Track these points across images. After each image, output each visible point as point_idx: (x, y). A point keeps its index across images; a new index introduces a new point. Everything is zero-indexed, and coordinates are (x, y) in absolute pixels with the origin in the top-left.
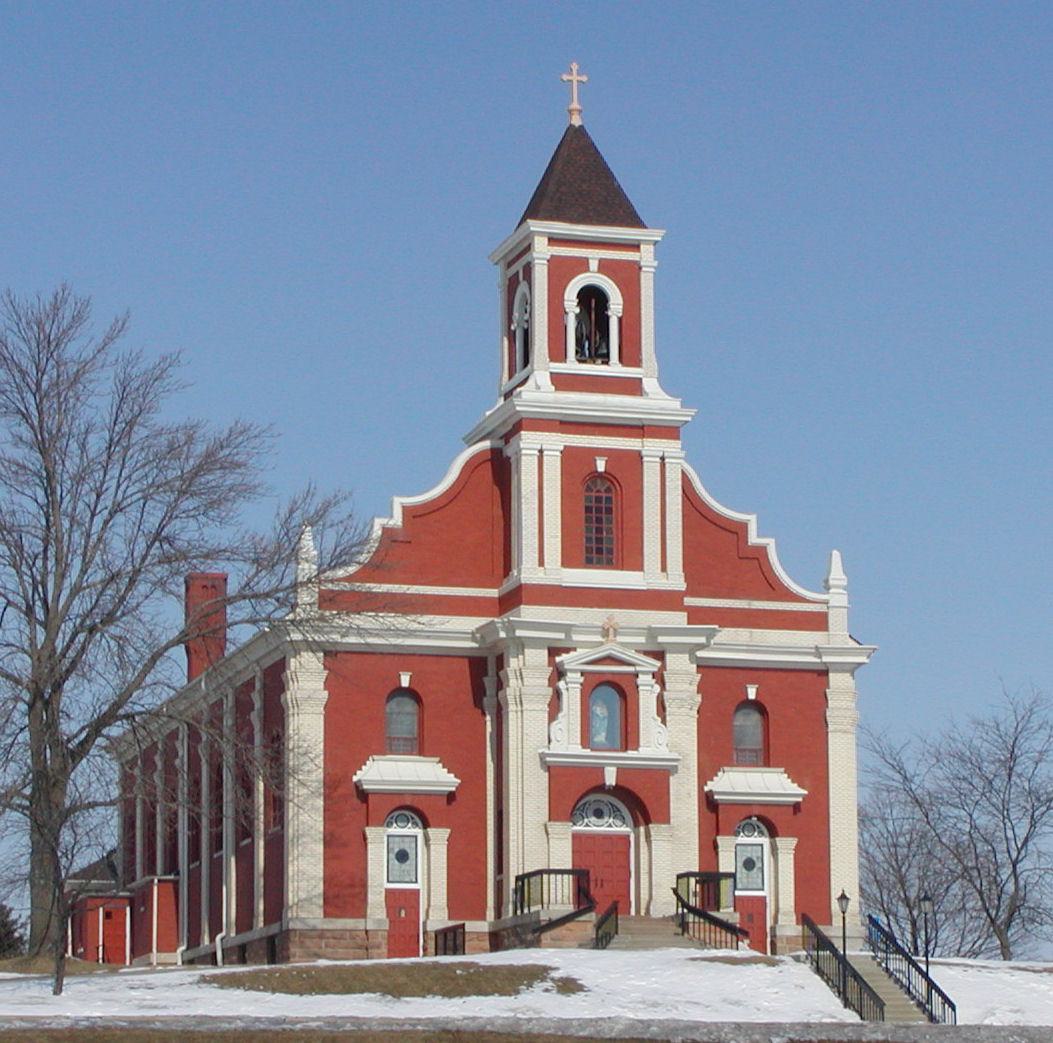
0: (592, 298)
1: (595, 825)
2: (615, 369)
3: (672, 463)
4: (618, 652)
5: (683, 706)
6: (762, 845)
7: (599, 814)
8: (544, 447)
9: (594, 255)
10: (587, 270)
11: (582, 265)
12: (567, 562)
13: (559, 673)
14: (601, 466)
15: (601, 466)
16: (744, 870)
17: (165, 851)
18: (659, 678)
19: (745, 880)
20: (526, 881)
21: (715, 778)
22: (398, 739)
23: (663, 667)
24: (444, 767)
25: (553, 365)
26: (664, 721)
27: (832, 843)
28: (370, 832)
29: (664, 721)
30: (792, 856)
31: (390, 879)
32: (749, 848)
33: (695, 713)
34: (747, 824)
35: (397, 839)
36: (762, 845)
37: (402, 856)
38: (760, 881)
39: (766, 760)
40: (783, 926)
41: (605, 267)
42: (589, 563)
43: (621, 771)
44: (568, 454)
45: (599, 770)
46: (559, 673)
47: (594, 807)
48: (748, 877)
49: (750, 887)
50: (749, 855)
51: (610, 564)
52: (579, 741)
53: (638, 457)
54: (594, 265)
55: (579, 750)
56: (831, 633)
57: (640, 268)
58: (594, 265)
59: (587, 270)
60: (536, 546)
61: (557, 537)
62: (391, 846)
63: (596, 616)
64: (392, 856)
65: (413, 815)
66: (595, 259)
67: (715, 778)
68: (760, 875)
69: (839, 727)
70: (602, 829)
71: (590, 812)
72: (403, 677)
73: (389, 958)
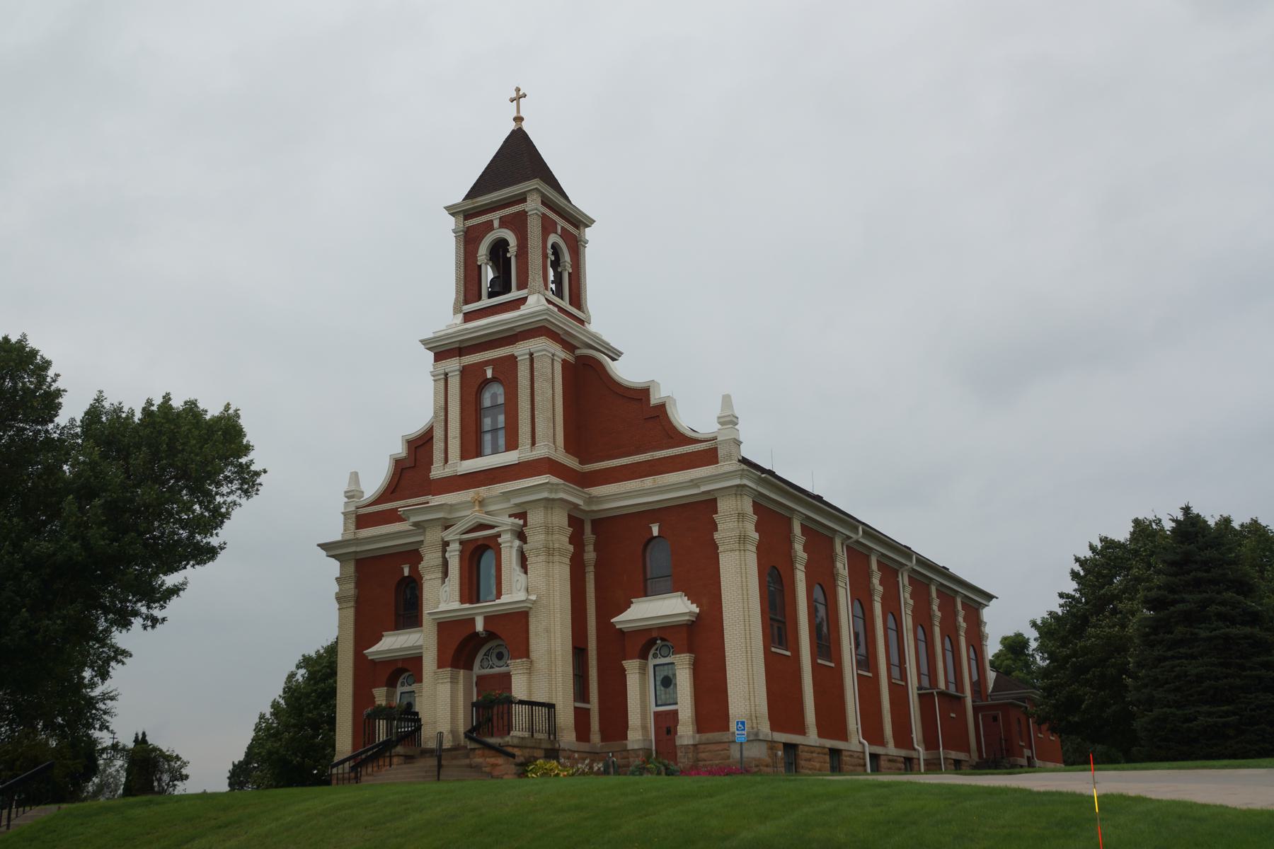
0: (499, 248)
6: (655, 666)
9: (495, 217)
11: (489, 226)
16: (662, 688)
18: (521, 536)
19: (663, 697)
20: (893, 681)
23: (525, 524)
24: (688, 599)
28: (626, 664)
29: (526, 573)
31: (659, 703)
32: (666, 667)
33: (568, 561)
40: (681, 737)
41: (504, 223)
43: (488, 619)
44: (465, 372)
45: (472, 621)
48: (666, 694)
49: (668, 702)
50: (666, 674)
54: (496, 224)
55: (456, 605)
56: (354, 515)
58: (496, 224)
61: (456, 437)
67: (690, 602)
69: (727, 547)
71: (494, 657)
73: (924, 760)
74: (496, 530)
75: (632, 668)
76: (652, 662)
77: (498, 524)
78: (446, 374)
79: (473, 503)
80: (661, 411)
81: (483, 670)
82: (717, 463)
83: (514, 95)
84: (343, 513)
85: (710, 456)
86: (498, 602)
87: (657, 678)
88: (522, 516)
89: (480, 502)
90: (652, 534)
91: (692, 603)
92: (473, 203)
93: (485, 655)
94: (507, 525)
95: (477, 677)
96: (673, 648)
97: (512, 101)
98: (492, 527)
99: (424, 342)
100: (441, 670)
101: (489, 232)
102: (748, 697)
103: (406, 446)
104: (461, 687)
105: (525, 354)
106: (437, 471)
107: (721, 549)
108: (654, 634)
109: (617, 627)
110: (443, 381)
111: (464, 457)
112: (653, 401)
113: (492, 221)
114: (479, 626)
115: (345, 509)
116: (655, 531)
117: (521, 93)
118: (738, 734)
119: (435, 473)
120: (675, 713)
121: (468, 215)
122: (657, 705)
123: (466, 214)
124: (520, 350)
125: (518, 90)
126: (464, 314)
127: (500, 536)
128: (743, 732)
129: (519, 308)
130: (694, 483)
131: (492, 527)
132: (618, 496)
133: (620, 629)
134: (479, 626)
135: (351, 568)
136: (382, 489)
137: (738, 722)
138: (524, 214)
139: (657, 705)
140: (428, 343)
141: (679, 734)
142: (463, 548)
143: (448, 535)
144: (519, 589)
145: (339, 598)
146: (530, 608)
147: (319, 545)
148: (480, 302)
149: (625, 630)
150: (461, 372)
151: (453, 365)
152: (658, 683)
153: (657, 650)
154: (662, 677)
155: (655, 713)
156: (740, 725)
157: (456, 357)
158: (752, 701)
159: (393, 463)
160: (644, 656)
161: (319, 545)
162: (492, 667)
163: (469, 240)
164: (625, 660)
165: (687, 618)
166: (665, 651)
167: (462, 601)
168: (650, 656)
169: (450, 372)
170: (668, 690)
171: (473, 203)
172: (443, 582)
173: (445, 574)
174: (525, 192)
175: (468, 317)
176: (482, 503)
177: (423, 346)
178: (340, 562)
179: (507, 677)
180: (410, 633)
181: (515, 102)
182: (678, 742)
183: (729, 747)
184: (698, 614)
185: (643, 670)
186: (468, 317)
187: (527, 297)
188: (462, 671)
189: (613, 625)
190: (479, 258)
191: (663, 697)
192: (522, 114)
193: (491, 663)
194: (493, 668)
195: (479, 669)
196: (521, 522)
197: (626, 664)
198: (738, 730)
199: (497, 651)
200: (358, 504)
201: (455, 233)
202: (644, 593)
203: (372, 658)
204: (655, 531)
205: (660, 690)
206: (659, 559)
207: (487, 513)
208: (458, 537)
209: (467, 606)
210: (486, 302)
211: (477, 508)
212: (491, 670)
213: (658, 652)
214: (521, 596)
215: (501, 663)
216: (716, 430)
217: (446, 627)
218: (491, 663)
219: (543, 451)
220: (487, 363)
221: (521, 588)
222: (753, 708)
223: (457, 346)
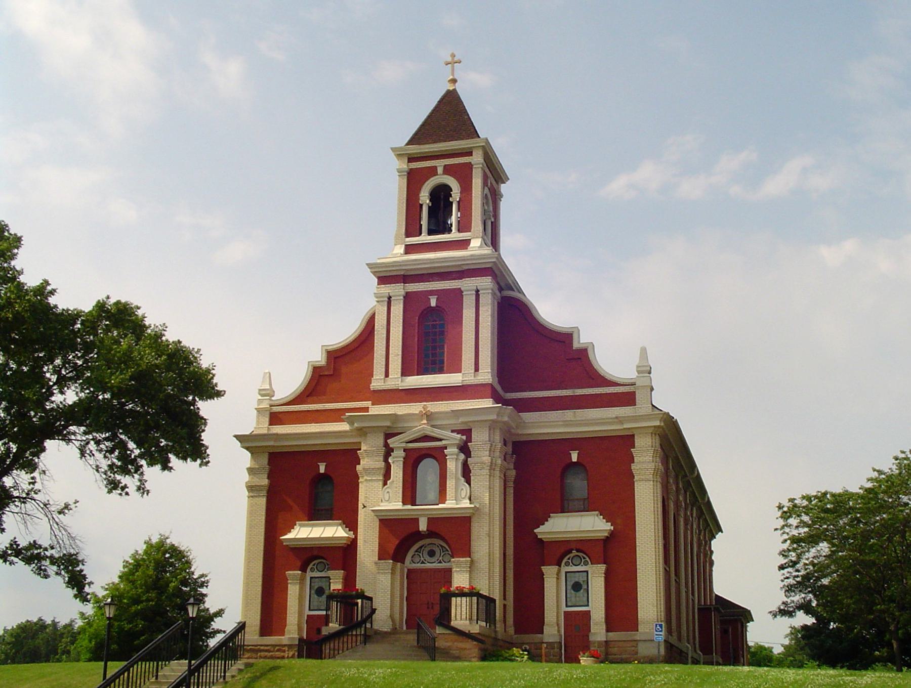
0: (441, 196)
1: (428, 562)
2: (454, 235)
3: (484, 293)
4: (436, 433)
5: (483, 468)
6: (311, 578)
7: (432, 554)
8: (391, 295)
9: (440, 164)
10: (436, 174)
11: (433, 171)
12: (405, 372)
13: (388, 451)
14: (433, 303)
15: (433, 303)
17: (701, 582)
18: (465, 449)
19: (573, 599)
21: (605, 520)
22: (322, 510)
25: (408, 239)
26: (385, 484)
27: (638, 567)
28: (545, 569)
30: (603, 579)
31: (569, 604)
34: (321, 562)
35: (317, 579)
36: (311, 578)
37: (577, 587)
38: (585, 599)
39: (588, 506)
40: (595, 634)
41: (448, 170)
42: (423, 370)
43: (431, 521)
44: (408, 298)
45: (416, 521)
46: (388, 451)
47: (428, 549)
50: (577, 580)
51: (441, 371)
52: (401, 500)
53: (459, 293)
54: (440, 170)
57: (472, 166)
58: (440, 170)
59: (436, 174)
60: (384, 363)
61: (398, 355)
62: (312, 584)
63: (415, 408)
64: (313, 592)
65: (585, 556)
66: (441, 166)
67: (605, 520)
68: (586, 595)
70: (434, 564)
72: (321, 467)
74: (444, 442)
75: (549, 572)
76: (565, 569)
77: (445, 438)
78: (390, 298)
79: (421, 416)
80: (583, 355)
81: (414, 564)
82: (635, 405)
83: (449, 59)
84: (256, 409)
85: (628, 399)
86: (441, 506)
87: (568, 583)
88: (467, 432)
89: (427, 416)
90: (571, 460)
91: (607, 522)
92: (420, 149)
93: (416, 551)
94: (456, 439)
95: (408, 570)
96: (328, 565)
97: (447, 64)
98: (441, 440)
99: (370, 266)
100: (383, 561)
101: (432, 177)
102: (655, 604)
103: (325, 355)
104: (398, 577)
105: (473, 290)
106: (378, 382)
107: (636, 478)
108: (573, 546)
109: (539, 537)
110: (474, 296)
111: (405, 372)
112: (576, 345)
113: (436, 167)
114: (423, 526)
115: (258, 405)
116: (574, 457)
117: (456, 59)
118: (657, 635)
119: (375, 384)
120: (587, 614)
121: (411, 159)
122: (567, 606)
123: (410, 157)
124: (467, 285)
125: (453, 56)
126: (406, 245)
127: (446, 448)
128: (661, 633)
129: (467, 249)
130: (619, 420)
131: (441, 440)
132: (552, 424)
133: (541, 540)
134: (423, 526)
135: (264, 460)
136: (299, 392)
137: (656, 625)
138: (469, 166)
139: (567, 606)
140: (374, 268)
141: (592, 631)
142: (406, 455)
143: (394, 442)
144: (463, 497)
145: (251, 488)
146: (474, 514)
147: (236, 436)
148: (420, 237)
149: (545, 540)
150: (404, 297)
151: (398, 290)
152: (569, 587)
153: (569, 559)
154: (572, 583)
155: (565, 612)
156: (658, 627)
157: (401, 283)
158: (659, 608)
159: (311, 369)
160: (303, 569)
161: (236, 436)
162: (423, 563)
163: (414, 180)
164: (544, 566)
165: (345, 542)
166: (576, 561)
167: (404, 503)
168: (308, 570)
169: (394, 296)
170: (578, 594)
171: (420, 149)
172: (385, 484)
173: (387, 475)
174: (471, 147)
175: (409, 249)
176: (429, 416)
177: (369, 270)
178: (252, 454)
179: (448, 572)
180: (325, 525)
181: (450, 65)
182: (592, 638)
183: (637, 644)
184: (613, 531)
185: (302, 580)
186: (409, 249)
187: (470, 240)
188: (399, 564)
189: (282, 541)
190: (421, 198)
191: (573, 599)
192: (456, 77)
193: (422, 559)
194: (424, 563)
195: (410, 563)
196: (464, 437)
197: (545, 569)
198: (656, 631)
199: (429, 549)
200: (271, 402)
201: (398, 172)
202: (563, 508)
203: (288, 544)
204: (574, 457)
205: (571, 593)
206: (578, 485)
207: (433, 426)
208: (404, 445)
209: (409, 507)
210: (425, 238)
211: (425, 422)
212: (439, 564)
213: (570, 561)
214: (466, 504)
215: (433, 560)
216: (635, 377)
217: (388, 523)
218: (422, 559)
219: (486, 377)
220: (432, 293)
221: (466, 495)
222: (659, 617)
223: (402, 273)
